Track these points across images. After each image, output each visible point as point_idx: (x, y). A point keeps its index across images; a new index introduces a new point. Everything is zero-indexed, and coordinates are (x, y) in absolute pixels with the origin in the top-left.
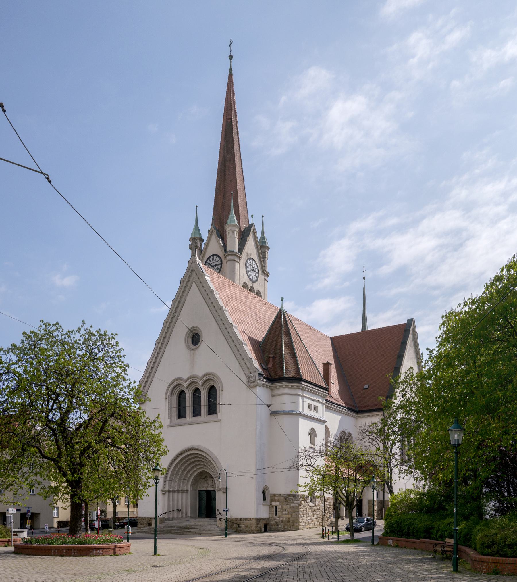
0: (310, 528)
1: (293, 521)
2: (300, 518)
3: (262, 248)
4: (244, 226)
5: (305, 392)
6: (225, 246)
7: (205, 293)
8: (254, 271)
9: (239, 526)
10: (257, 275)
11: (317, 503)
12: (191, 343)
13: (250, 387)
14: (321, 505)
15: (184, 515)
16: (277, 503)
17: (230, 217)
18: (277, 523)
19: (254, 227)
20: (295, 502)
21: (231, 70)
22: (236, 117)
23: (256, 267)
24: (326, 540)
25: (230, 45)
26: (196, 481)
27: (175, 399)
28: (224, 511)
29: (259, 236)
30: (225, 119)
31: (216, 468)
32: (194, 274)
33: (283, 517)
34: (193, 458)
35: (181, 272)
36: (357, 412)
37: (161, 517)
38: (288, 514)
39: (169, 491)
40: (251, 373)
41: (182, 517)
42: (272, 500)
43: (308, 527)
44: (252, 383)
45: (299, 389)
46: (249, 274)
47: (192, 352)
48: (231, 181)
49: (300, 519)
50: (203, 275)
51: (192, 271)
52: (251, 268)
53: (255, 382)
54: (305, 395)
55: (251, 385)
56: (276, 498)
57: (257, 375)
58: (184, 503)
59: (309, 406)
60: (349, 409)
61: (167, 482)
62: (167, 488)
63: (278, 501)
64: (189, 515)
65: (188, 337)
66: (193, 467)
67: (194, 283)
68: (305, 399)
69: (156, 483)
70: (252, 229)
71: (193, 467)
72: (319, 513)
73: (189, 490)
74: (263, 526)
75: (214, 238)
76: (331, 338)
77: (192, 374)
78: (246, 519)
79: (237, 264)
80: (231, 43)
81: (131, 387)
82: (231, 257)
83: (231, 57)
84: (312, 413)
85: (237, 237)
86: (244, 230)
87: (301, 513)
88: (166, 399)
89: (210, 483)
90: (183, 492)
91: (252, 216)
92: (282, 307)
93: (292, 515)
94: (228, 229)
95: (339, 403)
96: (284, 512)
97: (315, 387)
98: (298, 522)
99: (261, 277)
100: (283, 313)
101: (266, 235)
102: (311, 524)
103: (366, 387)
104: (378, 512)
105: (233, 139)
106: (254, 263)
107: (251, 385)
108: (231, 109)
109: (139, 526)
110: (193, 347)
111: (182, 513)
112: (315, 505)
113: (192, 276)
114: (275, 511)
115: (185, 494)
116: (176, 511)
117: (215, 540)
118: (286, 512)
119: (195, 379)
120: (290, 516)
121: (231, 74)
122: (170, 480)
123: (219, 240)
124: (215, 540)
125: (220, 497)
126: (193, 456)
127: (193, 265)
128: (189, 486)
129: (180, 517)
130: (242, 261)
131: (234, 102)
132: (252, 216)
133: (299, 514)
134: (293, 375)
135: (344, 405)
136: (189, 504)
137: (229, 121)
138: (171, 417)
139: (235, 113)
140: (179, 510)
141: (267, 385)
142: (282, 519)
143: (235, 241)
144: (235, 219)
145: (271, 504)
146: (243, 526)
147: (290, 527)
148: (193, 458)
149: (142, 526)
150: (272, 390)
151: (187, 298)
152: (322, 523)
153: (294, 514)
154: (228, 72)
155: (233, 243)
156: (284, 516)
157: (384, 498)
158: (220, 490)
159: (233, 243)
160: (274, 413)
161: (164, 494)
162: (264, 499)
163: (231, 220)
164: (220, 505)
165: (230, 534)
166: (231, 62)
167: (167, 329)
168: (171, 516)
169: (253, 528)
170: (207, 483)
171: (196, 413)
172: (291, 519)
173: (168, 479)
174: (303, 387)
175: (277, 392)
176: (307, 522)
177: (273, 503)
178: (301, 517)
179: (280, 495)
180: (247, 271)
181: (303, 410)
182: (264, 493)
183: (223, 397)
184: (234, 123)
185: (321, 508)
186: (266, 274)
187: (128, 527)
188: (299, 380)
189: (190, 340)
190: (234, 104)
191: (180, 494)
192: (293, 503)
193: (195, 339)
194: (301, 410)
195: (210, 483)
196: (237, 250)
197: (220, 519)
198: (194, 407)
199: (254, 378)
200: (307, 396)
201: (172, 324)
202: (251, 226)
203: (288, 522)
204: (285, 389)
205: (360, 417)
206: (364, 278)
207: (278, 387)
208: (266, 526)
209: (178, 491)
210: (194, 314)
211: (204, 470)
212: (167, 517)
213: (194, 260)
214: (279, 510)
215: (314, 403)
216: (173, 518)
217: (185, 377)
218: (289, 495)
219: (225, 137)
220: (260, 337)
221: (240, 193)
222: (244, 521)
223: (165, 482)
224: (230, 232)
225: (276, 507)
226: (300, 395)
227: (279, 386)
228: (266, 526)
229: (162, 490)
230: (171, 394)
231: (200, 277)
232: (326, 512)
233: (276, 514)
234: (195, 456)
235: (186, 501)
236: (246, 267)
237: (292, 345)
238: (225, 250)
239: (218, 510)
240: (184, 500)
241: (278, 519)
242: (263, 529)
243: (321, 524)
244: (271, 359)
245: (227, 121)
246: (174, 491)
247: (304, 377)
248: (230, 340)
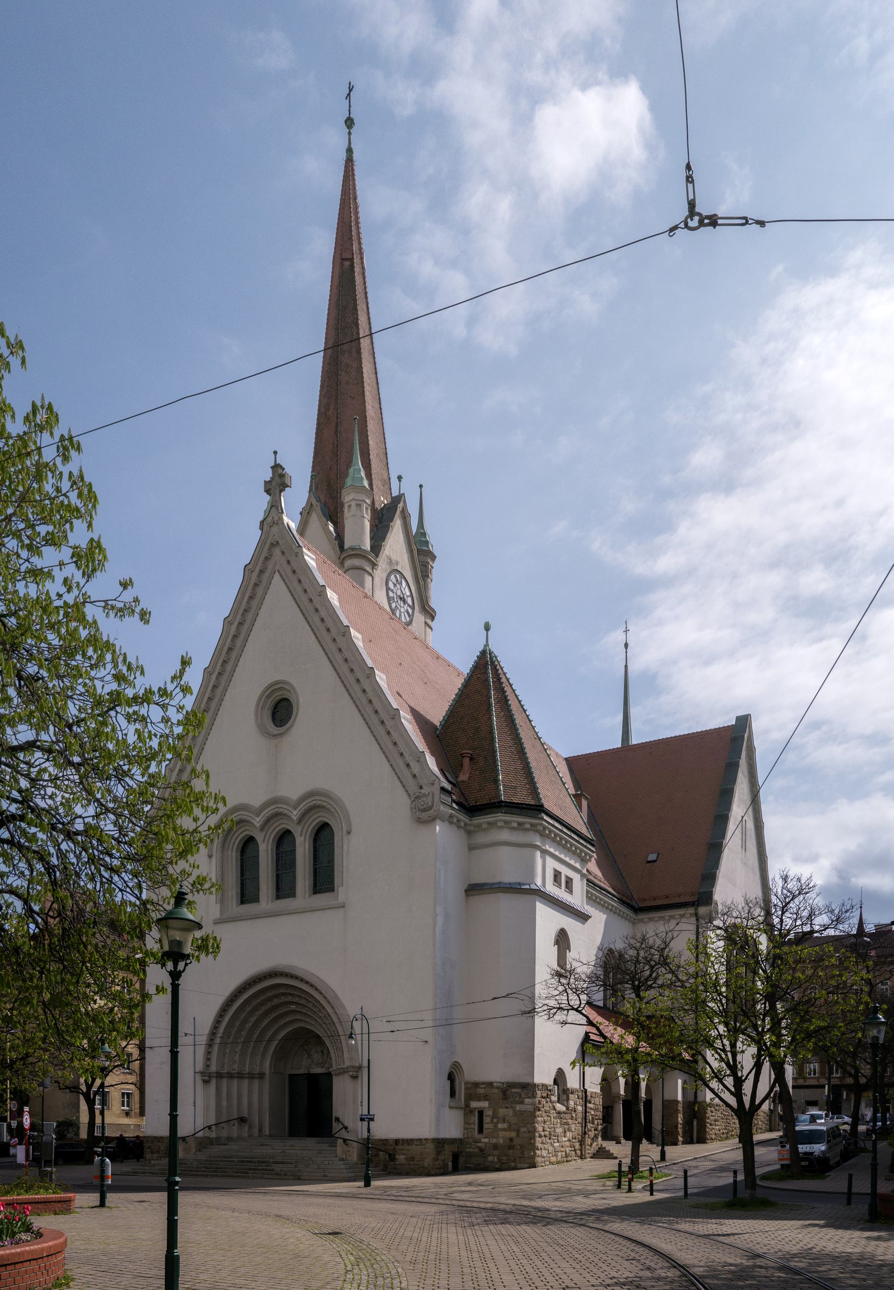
0: (558, 1163)
1: (522, 1146)
2: (537, 1139)
3: (422, 555)
4: (382, 500)
5: (548, 841)
6: (340, 538)
7: (304, 599)
8: (405, 602)
9: (392, 1157)
10: (410, 611)
11: (572, 1103)
12: (273, 726)
13: (421, 821)
14: (580, 1108)
15: (256, 1131)
16: (485, 1104)
17: (351, 471)
18: (481, 1150)
19: (405, 502)
20: (527, 1100)
21: (350, 151)
22: (362, 258)
23: (408, 593)
24: (640, 1196)
25: (349, 95)
26: (282, 1054)
27: (233, 855)
28: (362, 1120)
29: (414, 529)
30: (338, 260)
31: (335, 1019)
32: (277, 552)
33: (498, 1137)
34: (276, 996)
35: (246, 541)
36: (637, 910)
37: (200, 1134)
38: (510, 1129)
39: (219, 1076)
40: (421, 787)
41: (250, 1136)
42: (470, 1097)
43: (553, 1159)
44: (424, 810)
45: (537, 831)
46: (393, 605)
48: (353, 398)
49: (538, 1141)
50: (299, 555)
51: (272, 544)
52: (399, 593)
53: (431, 808)
54: (547, 847)
55: (423, 815)
56: (481, 1091)
57: (437, 792)
58: (256, 1104)
59: (557, 875)
60: (622, 902)
61: (216, 1048)
62: (213, 1069)
63: (486, 1098)
64: (267, 1131)
65: (268, 697)
66: (276, 1019)
67: (277, 576)
68: (549, 859)
69: (175, 975)
70: (400, 505)
71: (276, 1019)
72: (576, 1128)
73: (267, 1071)
74: (451, 1159)
75: (315, 520)
76: (566, 759)
78: (409, 1142)
79: (368, 579)
80: (350, 90)
81: (148, 906)
82: (356, 562)
84: (560, 893)
85: (367, 516)
86: (382, 509)
87: (540, 1128)
88: (210, 857)
89: (316, 1057)
90: (251, 1076)
91: (400, 478)
92: (487, 645)
93: (518, 1131)
94: (348, 497)
95: (602, 885)
96: (500, 1126)
97: (569, 833)
98: (534, 1148)
99: (419, 618)
100: (491, 658)
101: (428, 528)
102: (559, 1154)
103: (652, 857)
104: (684, 1128)
105: (355, 305)
106: (404, 584)
107: (423, 815)
108: (351, 239)
109: (148, 1156)
111: (250, 1127)
112: (567, 1108)
113: (274, 553)
114: (476, 1122)
115: (256, 1082)
116: (236, 1122)
117: (338, 1195)
118: (505, 1126)
119: (283, 808)
120: (513, 1134)
121: (349, 161)
122: (223, 1044)
123: (327, 525)
124: (338, 1195)
125: (341, 1087)
126: (277, 992)
127: (275, 529)
128: (267, 1064)
129: (246, 1135)
130: (380, 573)
131: (357, 223)
132: (400, 478)
133: (535, 1128)
134: (521, 797)
136: (266, 1105)
137: (347, 263)
139: (360, 249)
140: (242, 1120)
141: (458, 821)
142: (495, 1141)
143: (363, 527)
144: (364, 476)
145: (467, 1106)
146: (401, 1158)
147: (515, 1161)
148: (276, 996)
149: (155, 1156)
150: (469, 833)
151: (261, 612)
152: (581, 1150)
153: (523, 1130)
154: (344, 155)
155: (360, 531)
156: (501, 1134)
157: (696, 1097)
158: (343, 1072)
159: (360, 531)
160: (473, 890)
161: (206, 1082)
162: (453, 1094)
163: (353, 478)
164: (345, 1099)
165: (379, 1177)
166: (350, 133)
167: (212, 691)
168: (224, 1134)
169: (428, 1162)
170: (309, 1056)
172: (517, 1141)
173: (218, 1040)
174: (545, 828)
176: (551, 1148)
177: (474, 1104)
178: (540, 1136)
179: (490, 1084)
180: (389, 598)
181: (544, 885)
182: (451, 1077)
183: (353, 855)
184: (357, 269)
185: (580, 1115)
186: (429, 613)
187: (103, 1161)
188: (538, 809)
189: (267, 714)
190: (358, 228)
191: (246, 1081)
192: (522, 1103)
193: (280, 710)
194: (539, 882)
195: (316, 1057)
196: (367, 545)
197: (345, 1140)
198: (277, 876)
199: (430, 798)
200: (552, 850)
201: (224, 679)
202: (398, 500)
203: (511, 1147)
204: (501, 830)
205: (641, 921)
206: (626, 645)
207: (484, 826)
208: (455, 1158)
209: (240, 1076)
210: (279, 651)
211: (302, 1025)
212: (213, 1135)
213: (276, 518)
214: (487, 1120)
215: (565, 871)
216: (229, 1139)
217: (256, 802)
218: (512, 1085)
219: (338, 300)
220: (437, 714)
221: (371, 426)
222: (406, 1147)
223: (209, 1053)
224: (353, 504)
225: (481, 1113)
226: (537, 847)
227: (489, 823)
228: (456, 1157)
229: (202, 1073)
230: (223, 846)
231: (293, 559)
232: (589, 1125)
233: (481, 1130)
234: (282, 991)
235: (258, 1099)
236: (388, 589)
237: (517, 730)
238: (341, 547)
239: (337, 1119)
240: (255, 1097)
241: (486, 1140)
242: (450, 1164)
243: (579, 1152)
244: (466, 761)
245: (342, 265)
246: (230, 1076)
247: (548, 804)
248: (369, 710)
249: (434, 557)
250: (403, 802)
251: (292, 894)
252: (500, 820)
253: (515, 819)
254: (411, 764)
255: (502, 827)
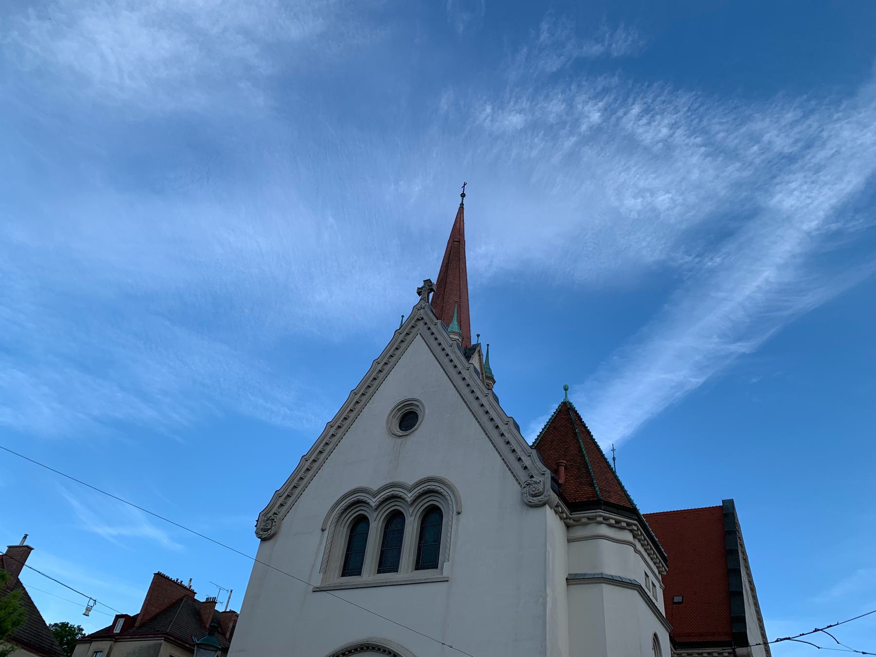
21: (462, 204)
47: (399, 440)
55: (534, 502)
65: (399, 410)
70: (478, 348)
77: (391, 481)
83: (463, 195)
88: (323, 530)
110: (400, 433)
132: (478, 336)
135: (661, 605)
138: (325, 569)
150: (568, 526)
171: (388, 562)
175: (579, 532)
183: (461, 536)
189: (396, 423)
193: (408, 418)
206: (864, 653)
230: (343, 513)
249: (494, 382)
250: (513, 489)
251: (395, 568)
252: (600, 516)
253: (613, 517)
254: (523, 458)
255: (600, 523)
